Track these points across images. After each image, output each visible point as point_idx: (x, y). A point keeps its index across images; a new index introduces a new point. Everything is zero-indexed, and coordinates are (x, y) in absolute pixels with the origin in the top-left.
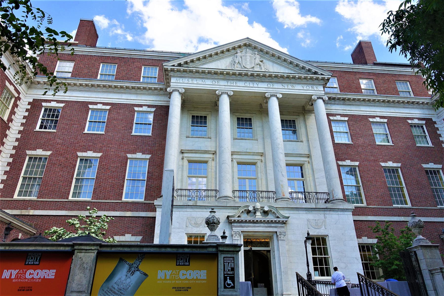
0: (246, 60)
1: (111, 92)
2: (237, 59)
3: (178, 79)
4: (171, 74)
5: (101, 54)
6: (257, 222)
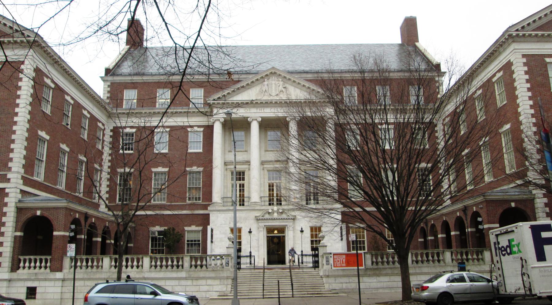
0: (271, 88)
6: (274, 219)
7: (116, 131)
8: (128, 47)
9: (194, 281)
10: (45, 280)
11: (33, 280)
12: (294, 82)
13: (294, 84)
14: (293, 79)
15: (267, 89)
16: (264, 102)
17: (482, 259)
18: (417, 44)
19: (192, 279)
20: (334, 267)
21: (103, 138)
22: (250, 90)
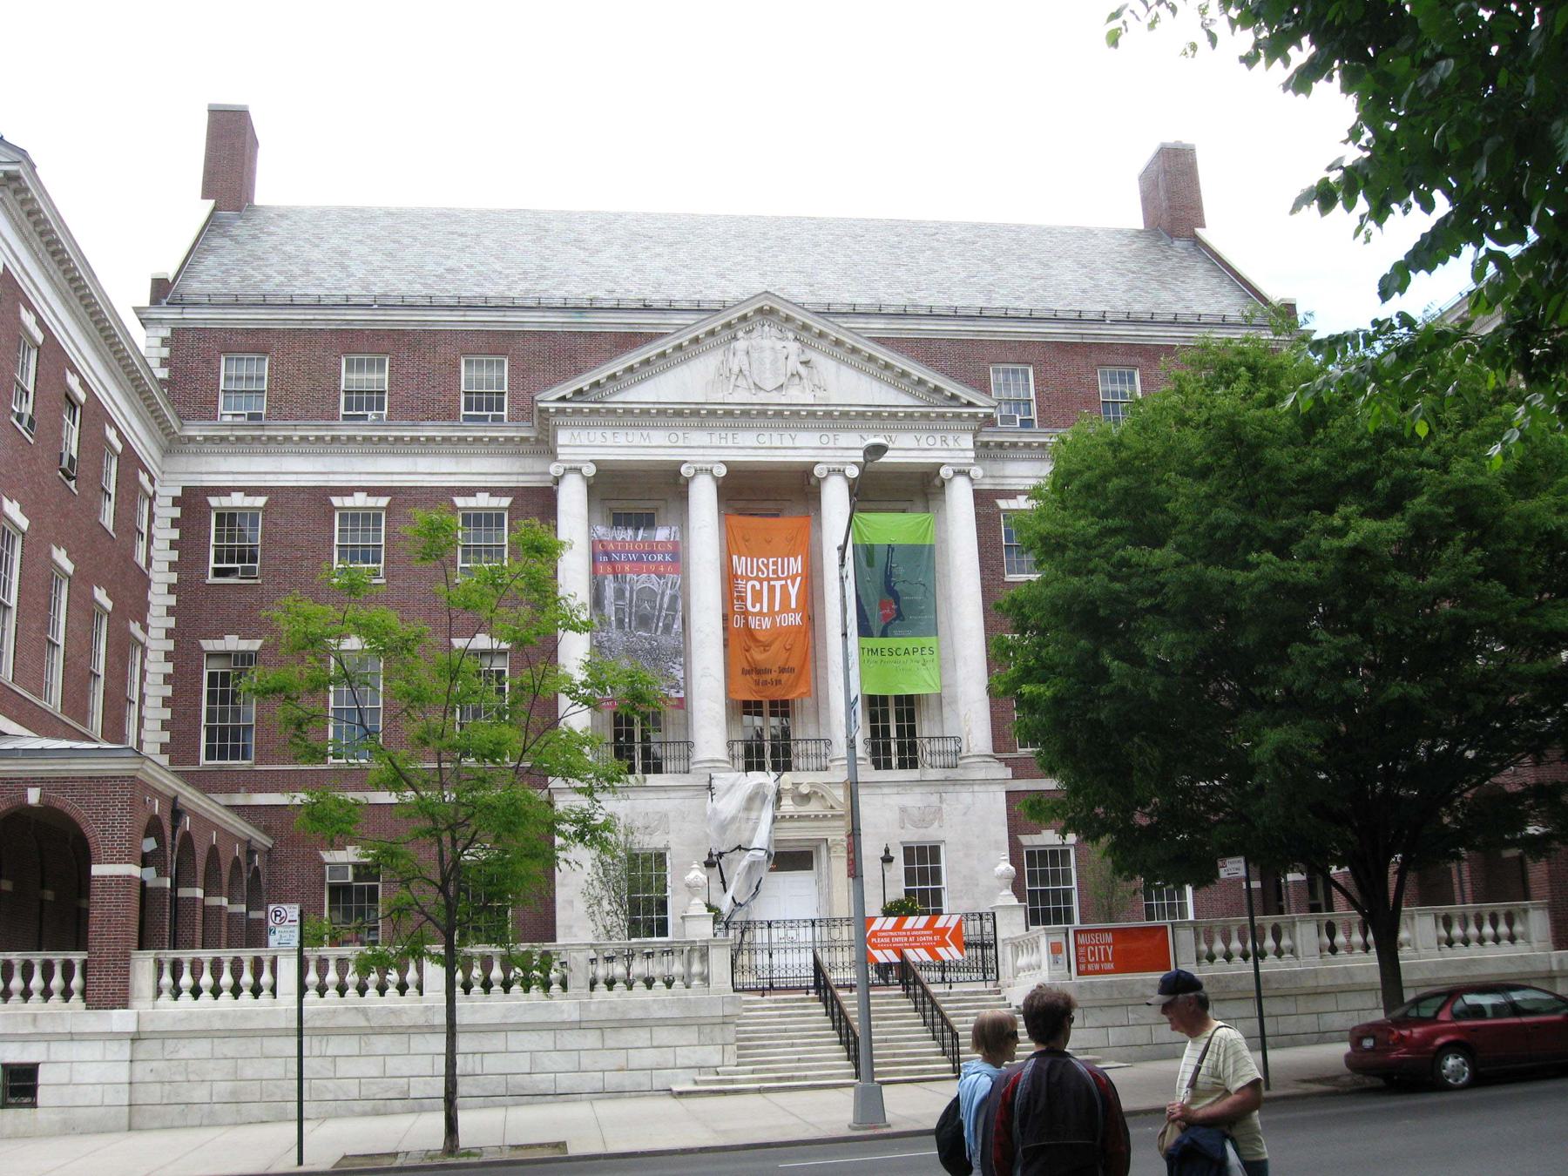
1: (383, 454)
2: (736, 360)
3: (576, 433)
4: (559, 420)
5: (339, 325)
7: (192, 501)
8: (211, 203)
9: (608, 1033)
10: (72, 1037)
11: (25, 1039)
12: (838, 343)
13: (837, 351)
14: (833, 335)
15: (745, 368)
16: (836, 411)
17: (1292, 951)
18: (1199, 231)
19: (602, 1027)
20: (1079, 973)
21: (149, 527)
22: (684, 367)
